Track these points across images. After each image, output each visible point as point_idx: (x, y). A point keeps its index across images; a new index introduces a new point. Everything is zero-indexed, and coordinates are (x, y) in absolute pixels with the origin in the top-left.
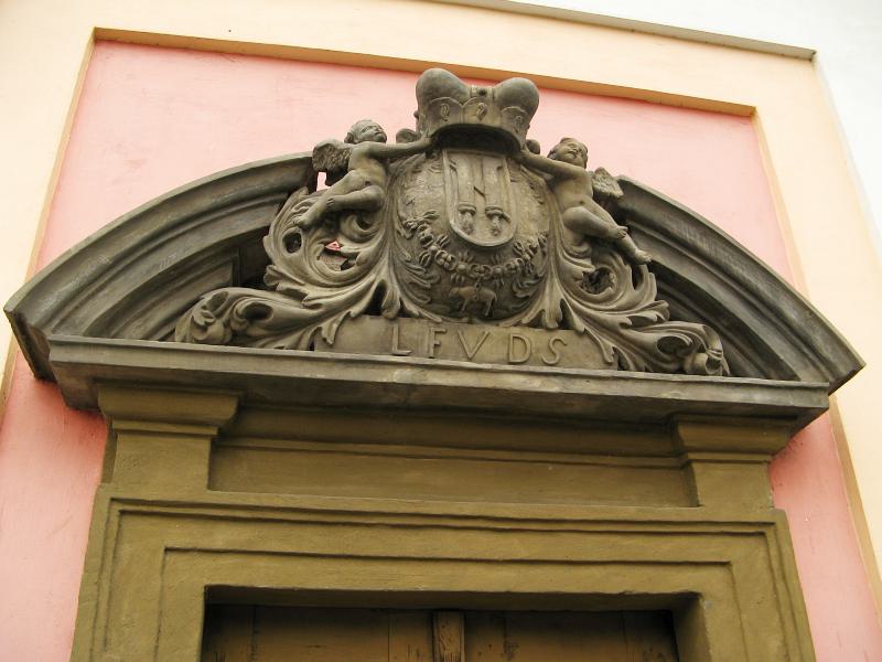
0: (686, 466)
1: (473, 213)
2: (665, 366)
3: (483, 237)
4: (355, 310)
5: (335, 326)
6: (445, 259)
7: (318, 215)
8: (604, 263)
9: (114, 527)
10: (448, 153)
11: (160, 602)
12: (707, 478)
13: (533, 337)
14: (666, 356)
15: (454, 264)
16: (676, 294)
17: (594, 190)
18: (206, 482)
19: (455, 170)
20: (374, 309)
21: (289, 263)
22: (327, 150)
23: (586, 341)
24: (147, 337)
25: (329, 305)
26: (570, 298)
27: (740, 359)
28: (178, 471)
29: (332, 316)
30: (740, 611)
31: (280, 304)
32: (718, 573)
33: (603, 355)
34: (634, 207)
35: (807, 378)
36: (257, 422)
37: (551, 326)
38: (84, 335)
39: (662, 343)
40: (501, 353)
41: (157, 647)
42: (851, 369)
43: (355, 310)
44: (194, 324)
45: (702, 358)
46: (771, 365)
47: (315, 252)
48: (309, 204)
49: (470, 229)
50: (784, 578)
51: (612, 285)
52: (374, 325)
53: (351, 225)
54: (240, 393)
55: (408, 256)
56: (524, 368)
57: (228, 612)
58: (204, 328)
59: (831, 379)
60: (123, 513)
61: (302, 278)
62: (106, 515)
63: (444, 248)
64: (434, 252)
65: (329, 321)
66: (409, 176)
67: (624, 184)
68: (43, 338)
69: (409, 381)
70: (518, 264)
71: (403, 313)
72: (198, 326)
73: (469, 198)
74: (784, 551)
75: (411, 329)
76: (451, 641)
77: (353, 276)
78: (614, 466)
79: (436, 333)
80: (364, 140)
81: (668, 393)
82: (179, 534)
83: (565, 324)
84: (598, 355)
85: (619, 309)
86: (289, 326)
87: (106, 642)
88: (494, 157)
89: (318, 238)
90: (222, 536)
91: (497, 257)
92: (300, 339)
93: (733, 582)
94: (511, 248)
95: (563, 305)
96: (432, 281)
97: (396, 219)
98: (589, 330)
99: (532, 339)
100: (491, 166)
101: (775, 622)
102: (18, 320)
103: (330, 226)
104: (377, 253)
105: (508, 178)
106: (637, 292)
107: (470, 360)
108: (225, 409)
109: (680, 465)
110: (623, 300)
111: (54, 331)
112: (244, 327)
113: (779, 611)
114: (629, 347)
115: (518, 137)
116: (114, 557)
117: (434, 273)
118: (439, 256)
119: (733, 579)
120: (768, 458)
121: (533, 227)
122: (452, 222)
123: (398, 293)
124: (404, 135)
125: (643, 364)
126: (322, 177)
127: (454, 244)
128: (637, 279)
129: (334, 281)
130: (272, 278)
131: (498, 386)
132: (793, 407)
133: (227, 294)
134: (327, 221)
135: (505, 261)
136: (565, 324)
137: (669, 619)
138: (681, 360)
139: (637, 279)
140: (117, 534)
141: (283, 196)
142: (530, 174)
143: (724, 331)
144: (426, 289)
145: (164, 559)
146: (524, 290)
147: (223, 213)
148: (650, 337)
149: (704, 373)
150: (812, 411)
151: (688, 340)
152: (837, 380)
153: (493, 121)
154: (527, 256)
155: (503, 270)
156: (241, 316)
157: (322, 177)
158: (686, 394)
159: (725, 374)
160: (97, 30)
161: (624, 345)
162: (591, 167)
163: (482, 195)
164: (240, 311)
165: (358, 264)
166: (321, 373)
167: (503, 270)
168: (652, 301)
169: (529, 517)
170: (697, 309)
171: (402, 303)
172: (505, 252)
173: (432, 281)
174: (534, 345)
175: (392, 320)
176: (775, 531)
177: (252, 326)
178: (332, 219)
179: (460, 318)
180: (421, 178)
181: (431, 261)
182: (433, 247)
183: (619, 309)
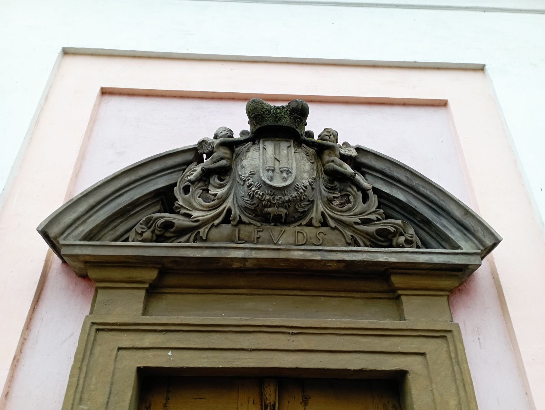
0: (398, 297)
1: (273, 171)
2: (380, 243)
3: (278, 183)
4: (216, 222)
5: (207, 230)
6: (259, 195)
7: (198, 175)
8: (347, 191)
9: (92, 338)
10: (263, 141)
11: (112, 377)
12: (409, 304)
13: (308, 230)
14: (379, 238)
15: (264, 197)
16: (391, 205)
17: (340, 154)
18: (141, 312)
19: (265, 149)
20: (226, 220)
21: (184, 200)
22: (203, 143)
23: (337, 232)
24: (116, 240)
25: (203, 220)
26: (327, 210)
27: (428, 238)
28: (127, 306)
29: (206, 225)
30: (431, 382)
31: (178, 220)
32: (419, 358)
33: (346, 240)
34: (363, 161)
35: (466, 246)
36: (171, 280)
37: (317, 225)
38: (80, 240)
39: (379, 232)
40: (291, 240)
41: (108, 402)
42: (493, 242)
43: (216, 222)
44: (137, 233)
45: (402, 239)
46: (444, 240)
47: (197, 194)
48: (195, 170)
49: (271, 179)
50: (459, 364)
51: (350, 202)
52: (226, 229)
53: (215, 180)
54: (160, 266)
55: (243, 193)
56: (302, 247)
57: (151, 382)
58: (141, 234)
59: (482, 248)
60: (98, 330)
61: (191, 207)
62: (88, 331)
63: (259, 189)
64: (254, 191)
65: (203, 228)
66: (244, 154)
67: (359, 149)
68: (58, 243)
69: (243, 256)
70: (297, 195)
71: (241, 222)
72: (139, 234)
73: (270, 163)
74: (458, 347)
75: (245, 230)
76: (271, 394)
77: (216, 205)
78: (358, 298)
79: (258, 231)
80: (221, 137)
81: (382, 258)
82: (126, 340)
83: (324, 224)
84: (343, 240)
85: (355, 215)
86: (183, 232)
87: (81, 400)
88: (287, 141)
89: (199, 187)
90: (148, 340)
91: (286, 192)
92: (190, 237)
93: (427, 365)
94: (293, 186)
95: (323, 214)
96: (255, 206)
97: (237, 176)
98: (338, 227)
99: (308, 233)
100: (284, 145)
101: (453, 391)
102: (44, 233)
103: (205, 181)
104: (228, 194)
105: (293, 151)
106: (365, 206)
107: (275, 244)
108: (152, 275)
109: (394, 296)
110: (358, 210)
111: (64, 239)
112: (162, 232)
113: (456, 383)
114: (360, 234)
115: (298, 130)
116: (91, 353)
117: (255, 201)
118: (256, 193)
119: (427, 363)
120: (447, 293)
121: (306, 176)
122: (262, 175)
123: (238, 213)
124: (243, 133)
125: (368, 243)
126: (205, 156)
127: (264, 187)
128: (365, 198)
129: (209, 207)
130: (177, 208)
131: (288, 257)
132: (458, 264)
133: (153, 217)
134: (204, 179)
135: (290, 193)
136: (324, 224)
137: (393, 384)
138: (391, 240)
139: (365, 198)
140: (93, 342)
141: (184, 167)
142: (308, 148)
143: (418, 223)
144: (252, 210)
145: (117, 354)
146: (303, 208)
147: (154, 177)
148: (371, 229)
149: (403, 247)
150: (470, 267)
151: (392, 229)
152: (486, 249)
153: (286, 122)
154: (302, 191)
155: (289, 199)
156: (159, 228)
157: (205, 156)
158: (393, 259)
159: (418, 247)
160: (102, 89)
161: (357, 233)
162: (340, 143)
163: (279, 161)
164: (159, 225)
165: (218, 199)
166: (206, 253)
167: (289, 199)
168: (374, 209)
169: (308, 326)
170: (402, 212)
171: (240, 217)
172: (290, 189)
173: (255, 206)
174: (308, 236)
175: (235, 226)
176: (453, 336)
177: (167, 232)
178: (206, 175)
179: (271, 223)
180: (249, 154)
181: (253, 196)
182: (253, 189)
183: (355, 215)
